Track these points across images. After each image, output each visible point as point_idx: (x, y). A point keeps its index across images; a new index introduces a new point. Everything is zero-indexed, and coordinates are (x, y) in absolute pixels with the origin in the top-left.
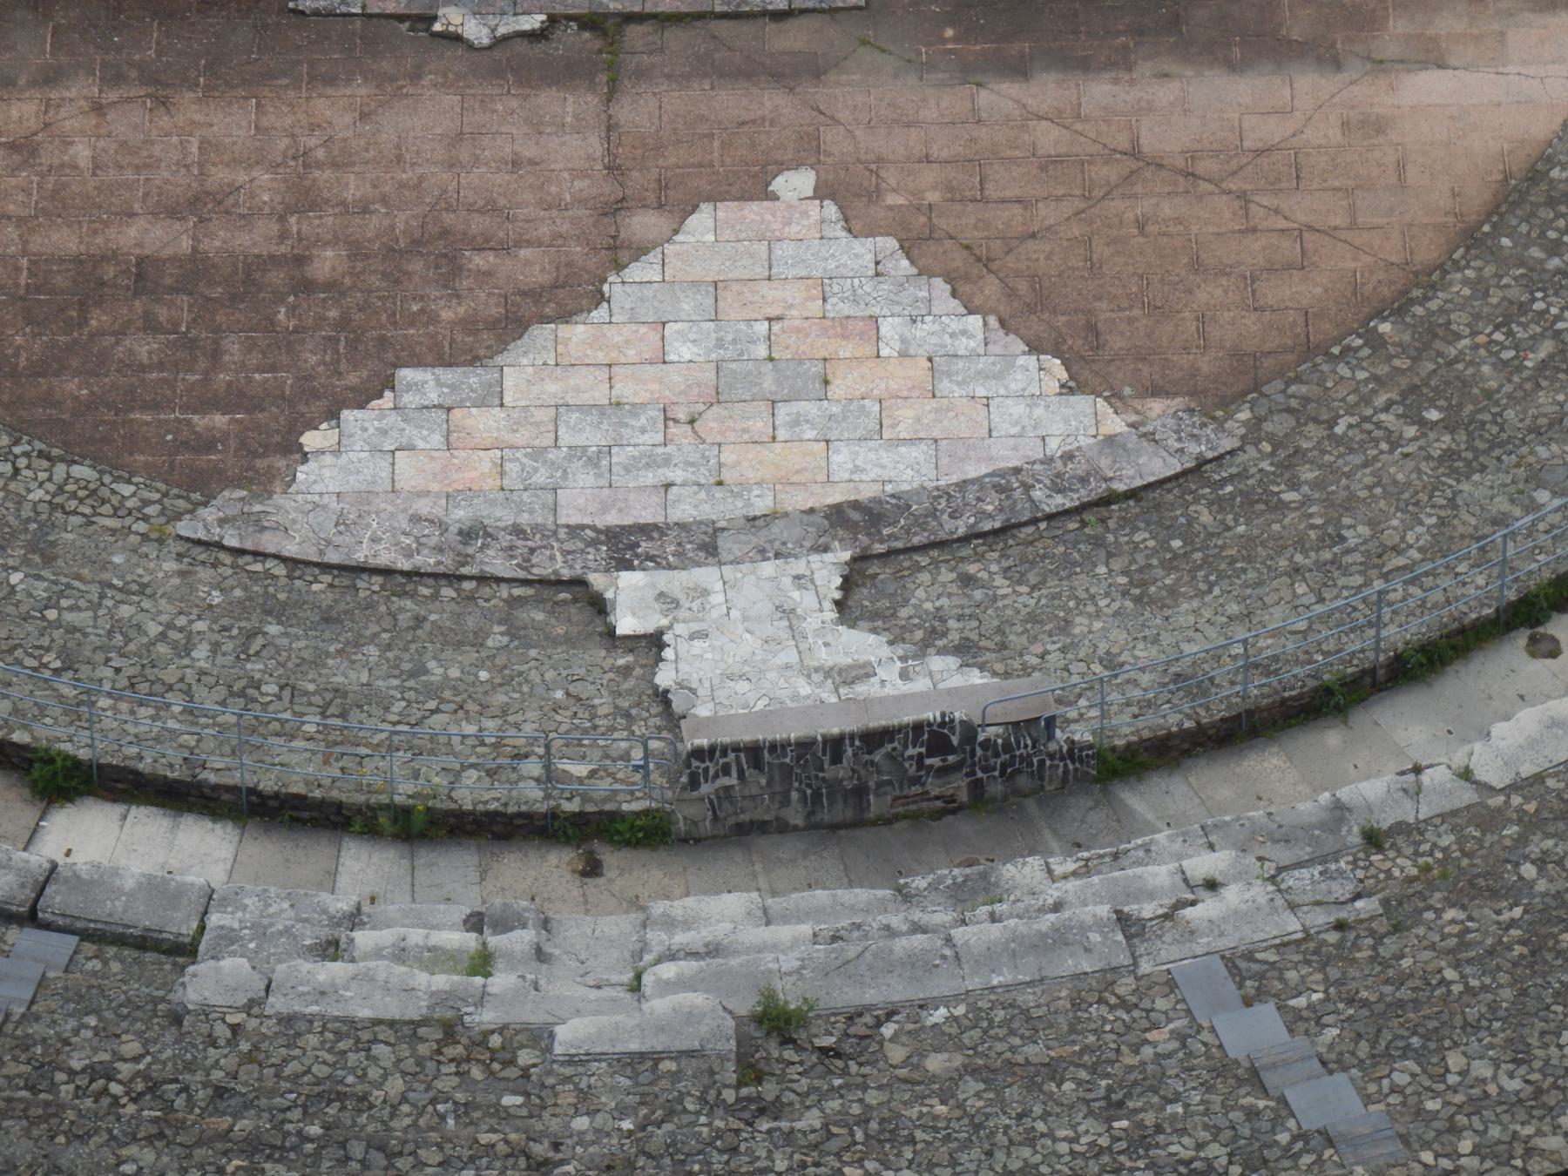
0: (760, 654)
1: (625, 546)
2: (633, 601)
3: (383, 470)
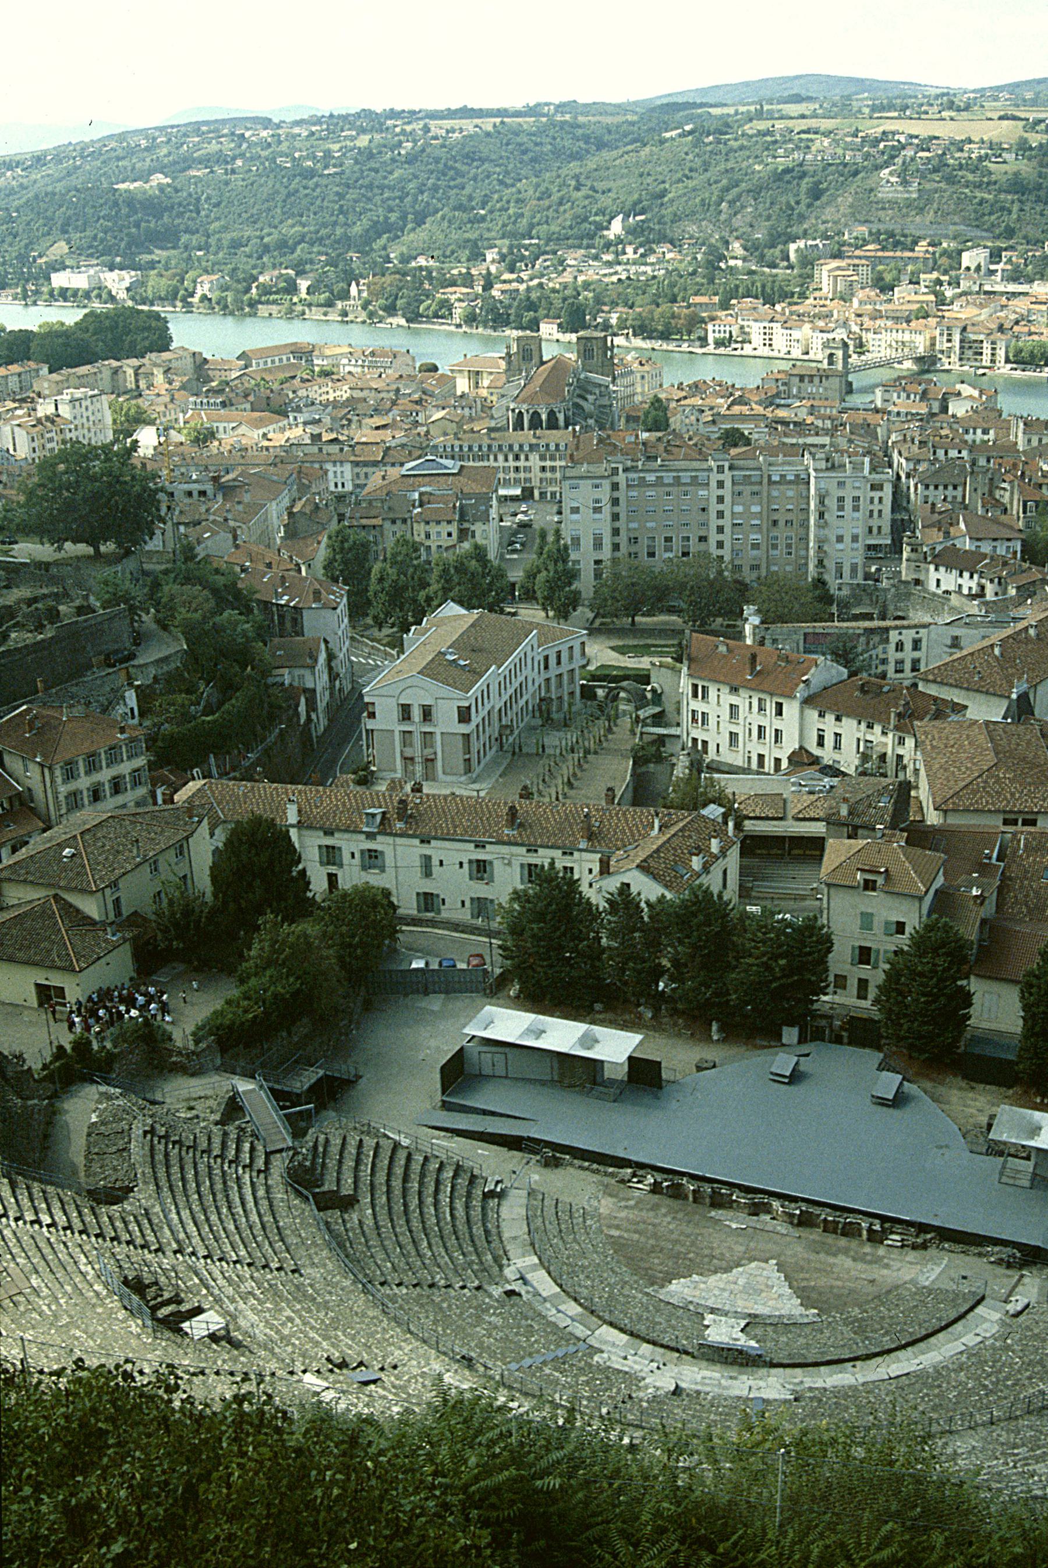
0: (722, 1332)
1: (713, 1311)
2: (709, 1319)
3: (679, 1289)
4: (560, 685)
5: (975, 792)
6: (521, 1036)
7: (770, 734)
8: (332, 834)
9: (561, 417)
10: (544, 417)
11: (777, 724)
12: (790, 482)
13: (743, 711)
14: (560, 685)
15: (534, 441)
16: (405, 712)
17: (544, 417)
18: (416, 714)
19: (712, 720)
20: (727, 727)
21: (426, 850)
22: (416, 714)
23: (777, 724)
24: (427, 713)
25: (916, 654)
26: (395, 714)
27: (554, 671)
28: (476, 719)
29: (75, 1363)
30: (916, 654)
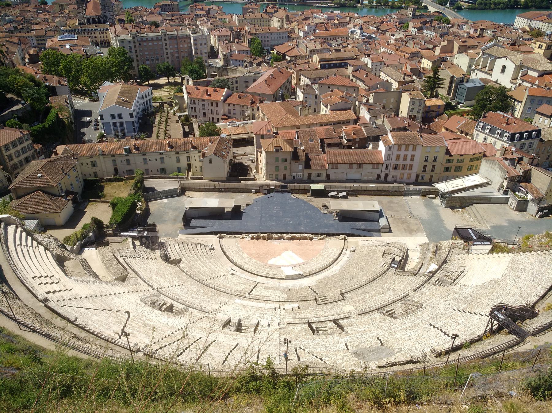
4: (147, 104)
5: (284, 122)
6: (219, 204)
7: (215, 112)
8: (145, 155)
9: (102, 19)
10: (97, 20)
11: (217, 109)
12: (150, 41)
13: (206, 106)
14: (147, 104)
15: (96, 28)
16: (113, 116)
17: (97, 20)
18: (116, 117)
19: (197, 110)
20: (202, 111)
21: (145, 157)
22: (116, 117)
23: (217, 109)
24: (120, 116)
25: (237, 85)
26: (110, 117)
27: (145, 100)
28: (134, 116)
29: (285, 343)
30: (237, 85)
